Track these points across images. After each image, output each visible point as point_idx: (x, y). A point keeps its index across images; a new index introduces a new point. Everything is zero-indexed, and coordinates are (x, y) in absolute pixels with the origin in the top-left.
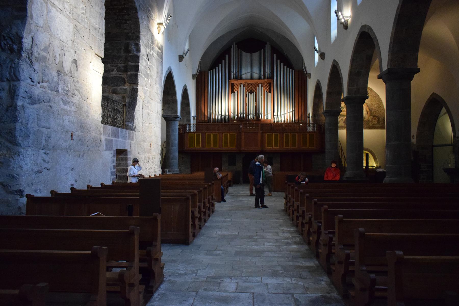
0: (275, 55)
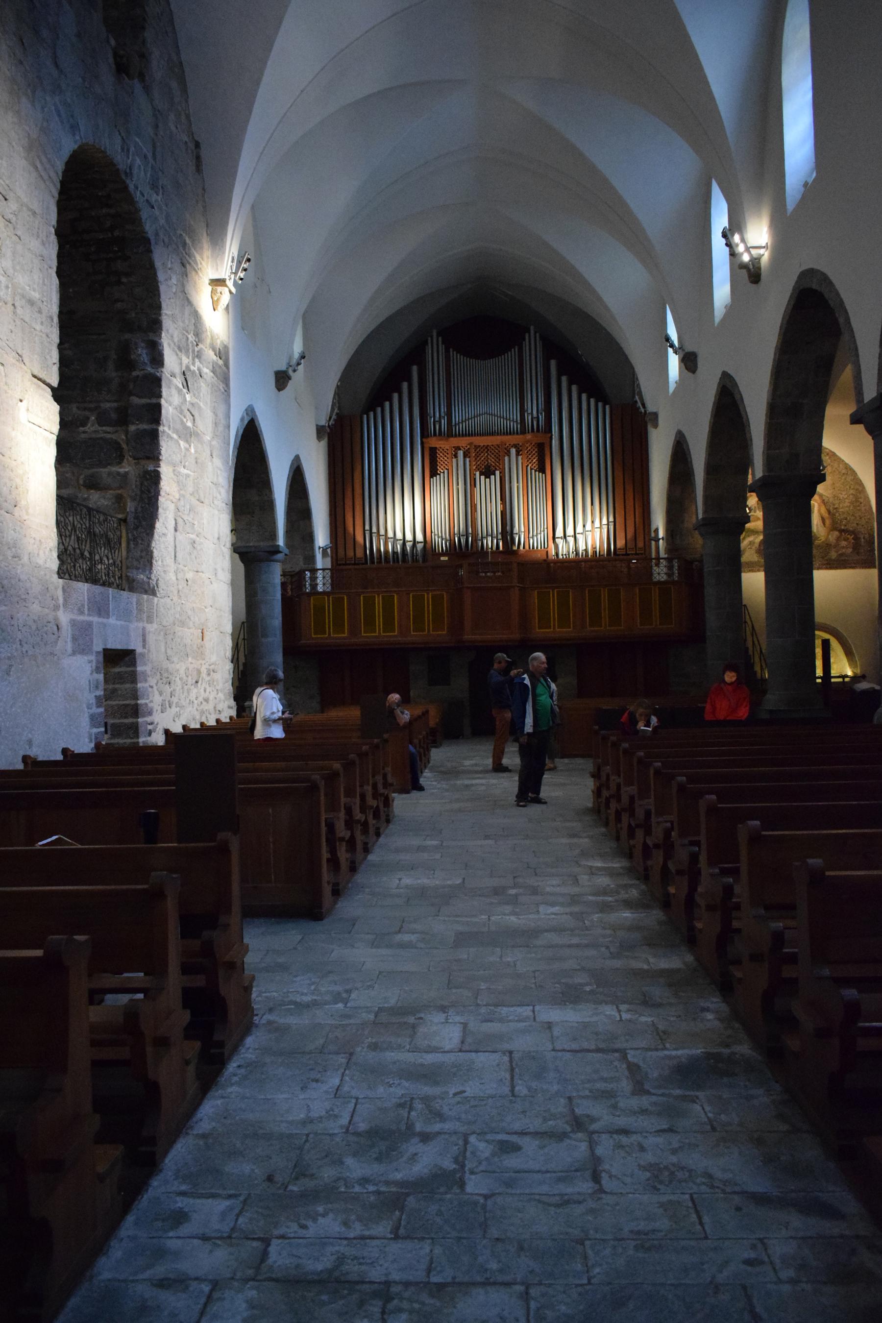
0: (553, 363)
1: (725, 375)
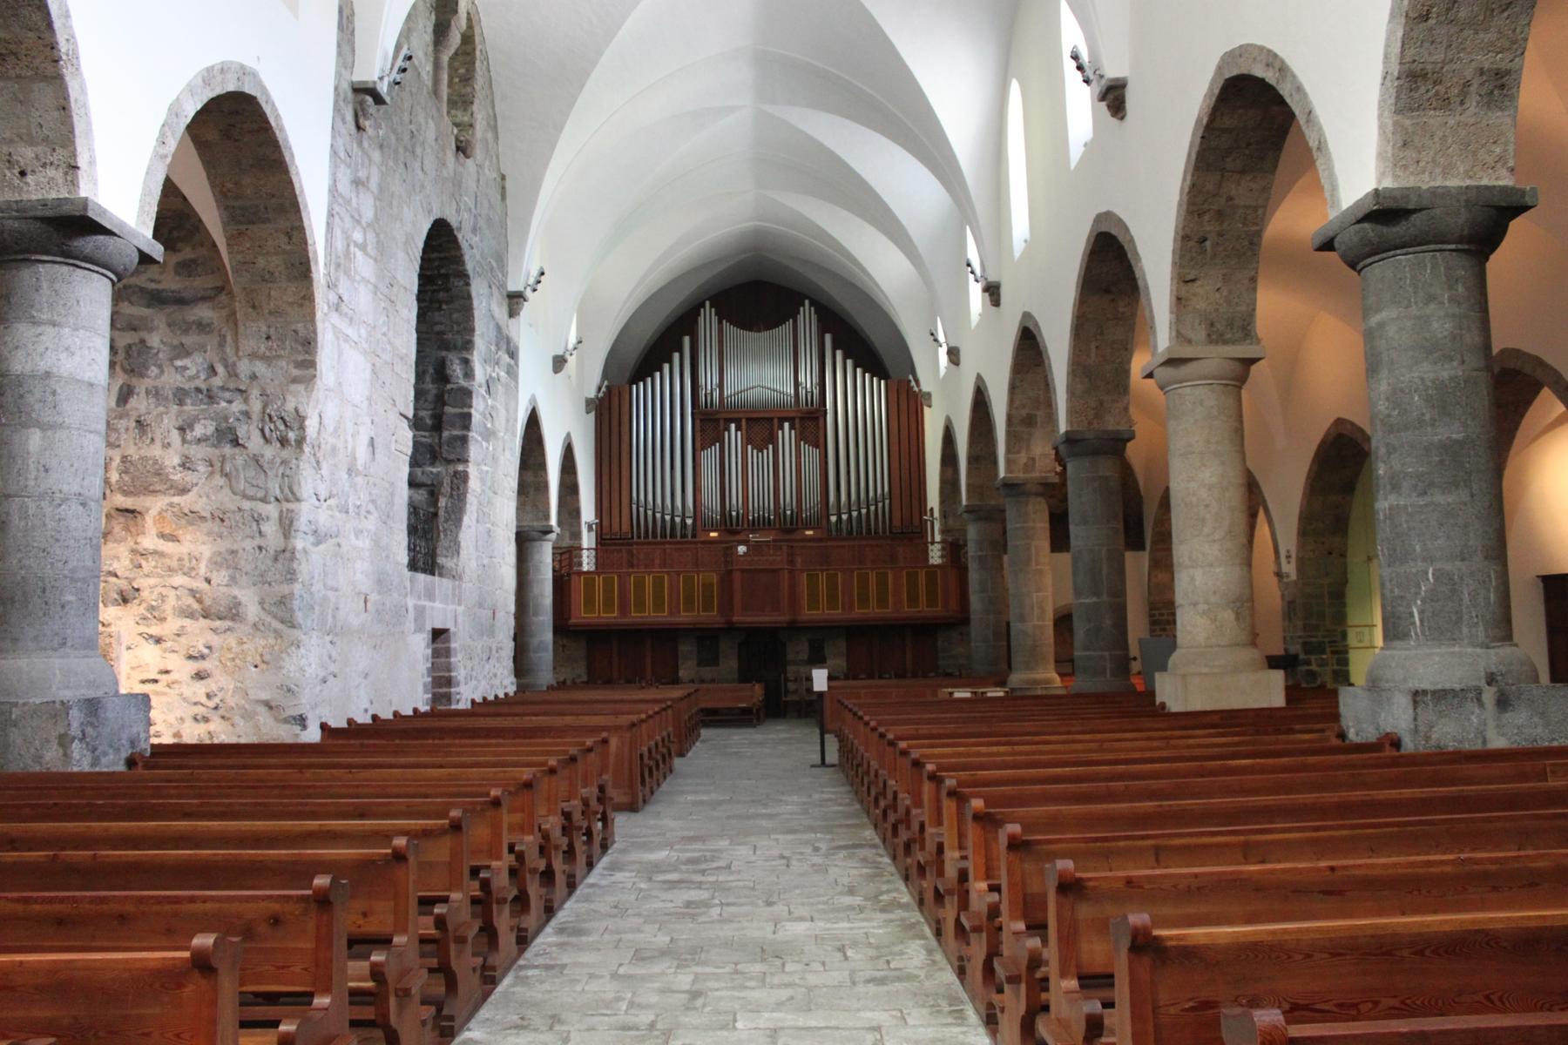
0: (828, 337)
1: (1027, 316)
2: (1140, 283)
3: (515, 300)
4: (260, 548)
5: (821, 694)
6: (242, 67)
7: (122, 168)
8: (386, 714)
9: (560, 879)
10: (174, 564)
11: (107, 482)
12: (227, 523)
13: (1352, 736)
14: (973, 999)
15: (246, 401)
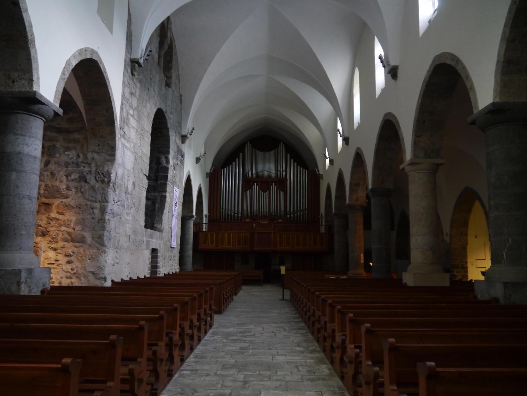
0: (289, 155)
1: (358, 148)
2: (400, 137)
3: (184, 138)
4: (93, 218)
5: (283, 275)
6: (93, 50)
7: (49, 83)
8: (135, 278)
9: (196, 338)
10: (62, 223)
11: (39, 193)
12: (82, 209)
13: (479, 297)
14: (347, 389)
15: (90, 167)
